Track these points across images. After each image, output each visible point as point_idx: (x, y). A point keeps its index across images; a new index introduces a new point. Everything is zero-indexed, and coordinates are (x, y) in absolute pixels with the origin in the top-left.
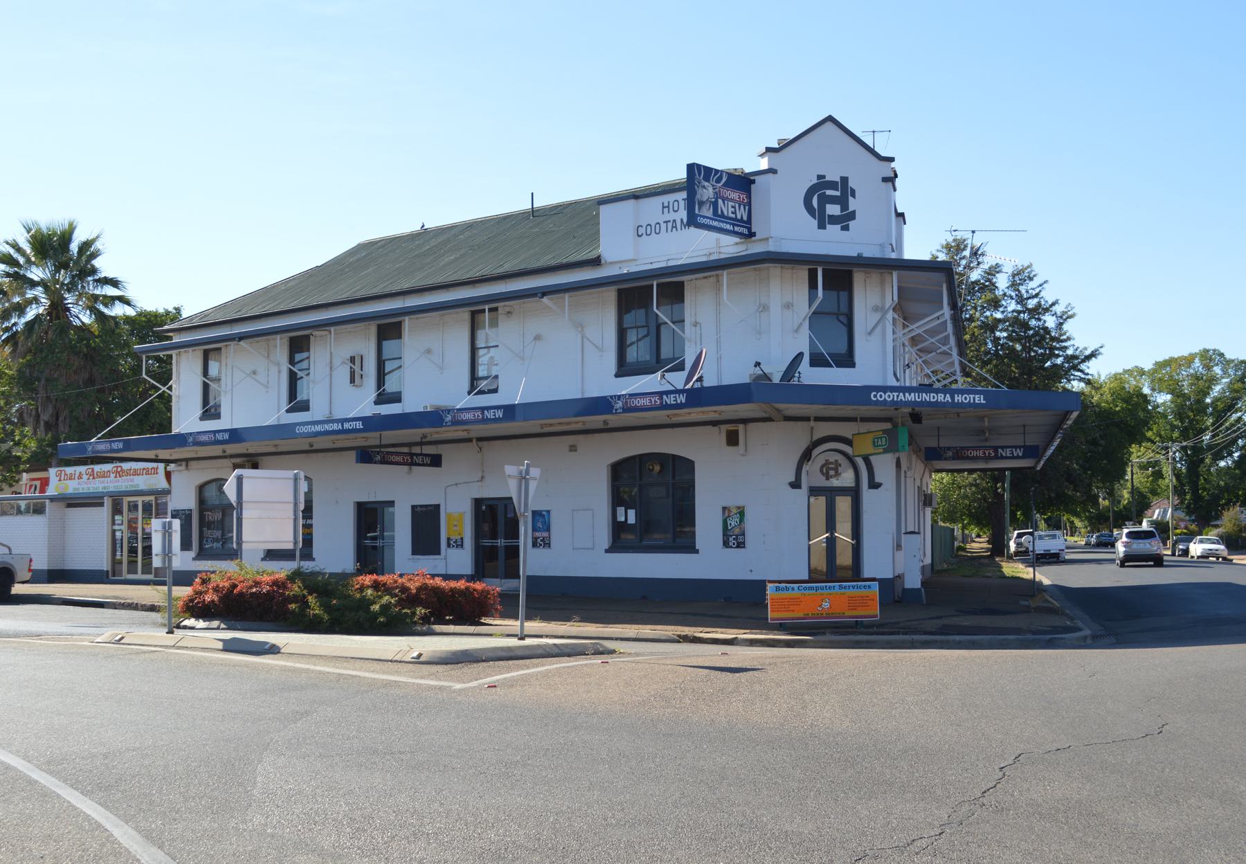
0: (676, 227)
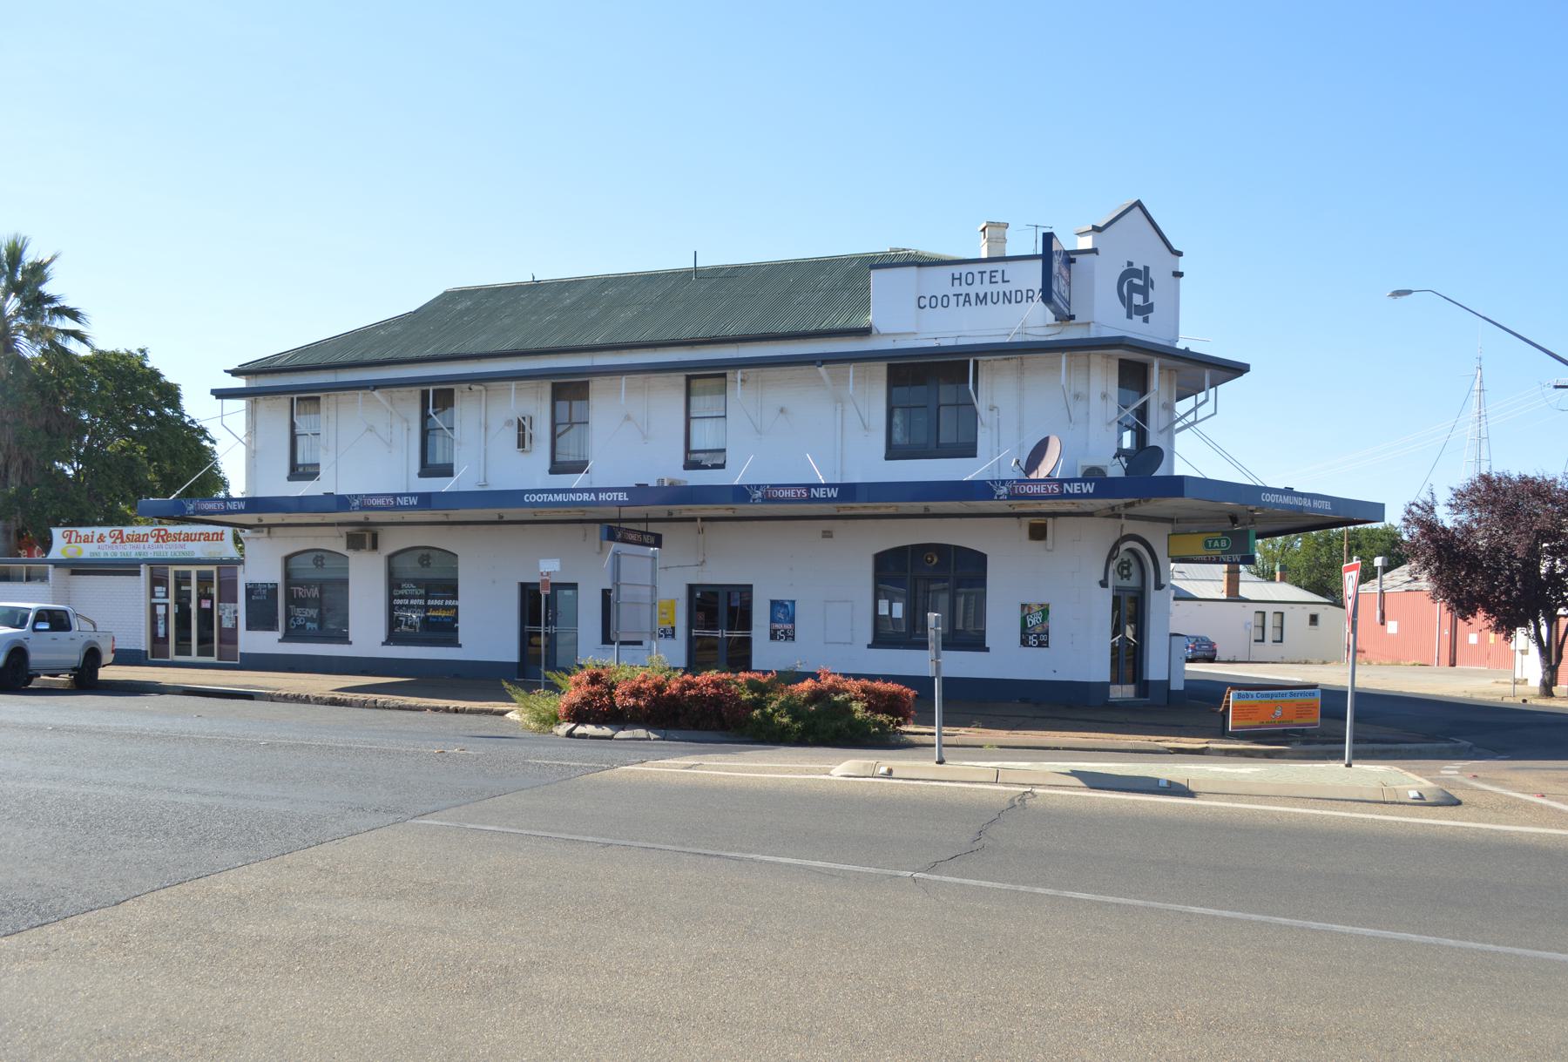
0: (969, 301)
